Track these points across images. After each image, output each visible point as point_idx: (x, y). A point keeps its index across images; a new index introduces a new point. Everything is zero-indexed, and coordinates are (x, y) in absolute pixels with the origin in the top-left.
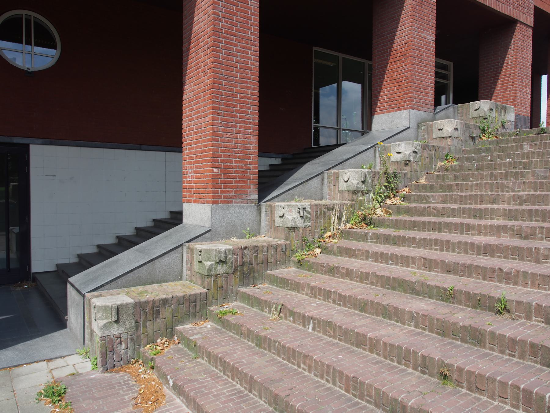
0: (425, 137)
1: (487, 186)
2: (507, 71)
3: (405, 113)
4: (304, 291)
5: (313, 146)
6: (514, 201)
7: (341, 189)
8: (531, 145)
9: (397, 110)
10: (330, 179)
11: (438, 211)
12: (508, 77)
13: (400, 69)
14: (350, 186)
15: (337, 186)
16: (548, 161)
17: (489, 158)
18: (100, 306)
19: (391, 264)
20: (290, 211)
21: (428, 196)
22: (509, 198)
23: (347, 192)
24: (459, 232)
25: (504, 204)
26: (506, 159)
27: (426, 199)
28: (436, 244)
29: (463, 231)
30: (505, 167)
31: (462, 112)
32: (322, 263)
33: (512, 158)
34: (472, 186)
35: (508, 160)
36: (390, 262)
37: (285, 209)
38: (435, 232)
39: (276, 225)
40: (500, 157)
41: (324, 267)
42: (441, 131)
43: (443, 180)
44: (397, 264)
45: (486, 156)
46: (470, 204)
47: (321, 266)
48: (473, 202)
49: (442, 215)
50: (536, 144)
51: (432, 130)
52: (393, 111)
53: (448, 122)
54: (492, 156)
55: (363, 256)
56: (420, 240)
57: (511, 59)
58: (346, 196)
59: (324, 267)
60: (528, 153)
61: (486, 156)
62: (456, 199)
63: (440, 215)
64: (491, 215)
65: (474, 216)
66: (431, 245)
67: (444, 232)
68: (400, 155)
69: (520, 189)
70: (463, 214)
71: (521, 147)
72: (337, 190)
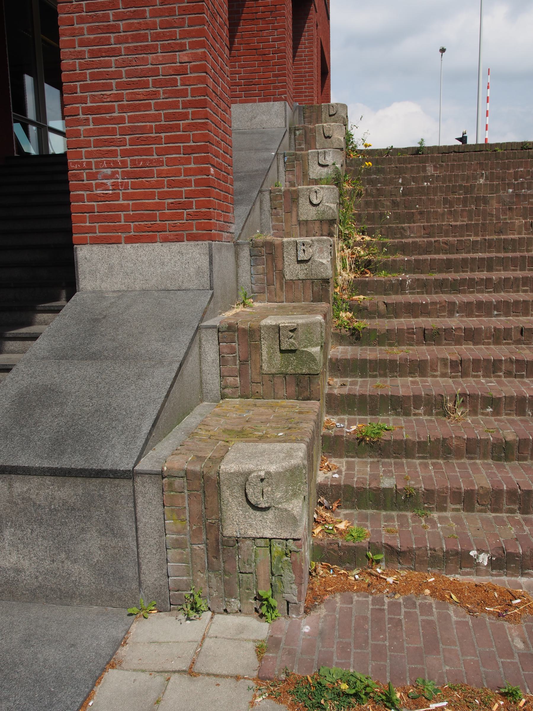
0: (303, 146)
1: (465, 214)
2: (301, 68)
3: (277, 107)
4: (436, 371)
5: (16, 155)
6: (526, 229)
7: (303, 218)
8: (435, 167)
9: (260, 101)
10: (276, 203)
11: (453, 245)
12: (301, 76)
13: (265, 33)
14: (324, 212)
15: (294, 214)
16: (531, 182)
17: (400, 181)
18: (280, 473)
19: (497, 315)
20: (321, 251)
21: (403, 228)
22: (520, 227)
23: (318, 224)
24: (518, 268)
25: (514, 234)
26: (423, 182)
27: (401, 233)
28: (524, 285)
29: (525, 267)
30: (442, 192)
31: (310, 117)
32: (408, 329)
33: (430, 182)
34: (443, 214)
35: (425, 184)
36: (496, 313)
37: (315, 248)
38: (483, 271)
39: (287, 277)
40: (414, 179)
41: (413, 333)
42: (328, 140)
43: (376, 208)
44: (507, 314)
45: (396, 178)
46: (468, 236)
47: (409, 333)
48: (472, 234)
49: (458, 251)
50: (441, 166)
51: (314, 137)
52: (255, 101)
53: (338, 126)
54: (404, 178)
55: (444, 312)
56: (499, 282)
57: (304, 52)
58: (316, 229)
59: (413, 333)
60: (432, 176)
61: (396, 178)
62: (447, 230)
63: (455, 251)
64: (528, 247)
65: (504, 248)
66: (518, 286)
67: (497, 270)
68: (325, 170)
69: (507, 217)
70: (490, 247)
71: (424, 169)
72: (294, 220)
